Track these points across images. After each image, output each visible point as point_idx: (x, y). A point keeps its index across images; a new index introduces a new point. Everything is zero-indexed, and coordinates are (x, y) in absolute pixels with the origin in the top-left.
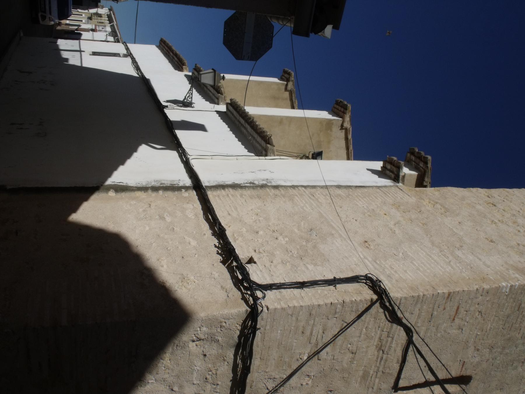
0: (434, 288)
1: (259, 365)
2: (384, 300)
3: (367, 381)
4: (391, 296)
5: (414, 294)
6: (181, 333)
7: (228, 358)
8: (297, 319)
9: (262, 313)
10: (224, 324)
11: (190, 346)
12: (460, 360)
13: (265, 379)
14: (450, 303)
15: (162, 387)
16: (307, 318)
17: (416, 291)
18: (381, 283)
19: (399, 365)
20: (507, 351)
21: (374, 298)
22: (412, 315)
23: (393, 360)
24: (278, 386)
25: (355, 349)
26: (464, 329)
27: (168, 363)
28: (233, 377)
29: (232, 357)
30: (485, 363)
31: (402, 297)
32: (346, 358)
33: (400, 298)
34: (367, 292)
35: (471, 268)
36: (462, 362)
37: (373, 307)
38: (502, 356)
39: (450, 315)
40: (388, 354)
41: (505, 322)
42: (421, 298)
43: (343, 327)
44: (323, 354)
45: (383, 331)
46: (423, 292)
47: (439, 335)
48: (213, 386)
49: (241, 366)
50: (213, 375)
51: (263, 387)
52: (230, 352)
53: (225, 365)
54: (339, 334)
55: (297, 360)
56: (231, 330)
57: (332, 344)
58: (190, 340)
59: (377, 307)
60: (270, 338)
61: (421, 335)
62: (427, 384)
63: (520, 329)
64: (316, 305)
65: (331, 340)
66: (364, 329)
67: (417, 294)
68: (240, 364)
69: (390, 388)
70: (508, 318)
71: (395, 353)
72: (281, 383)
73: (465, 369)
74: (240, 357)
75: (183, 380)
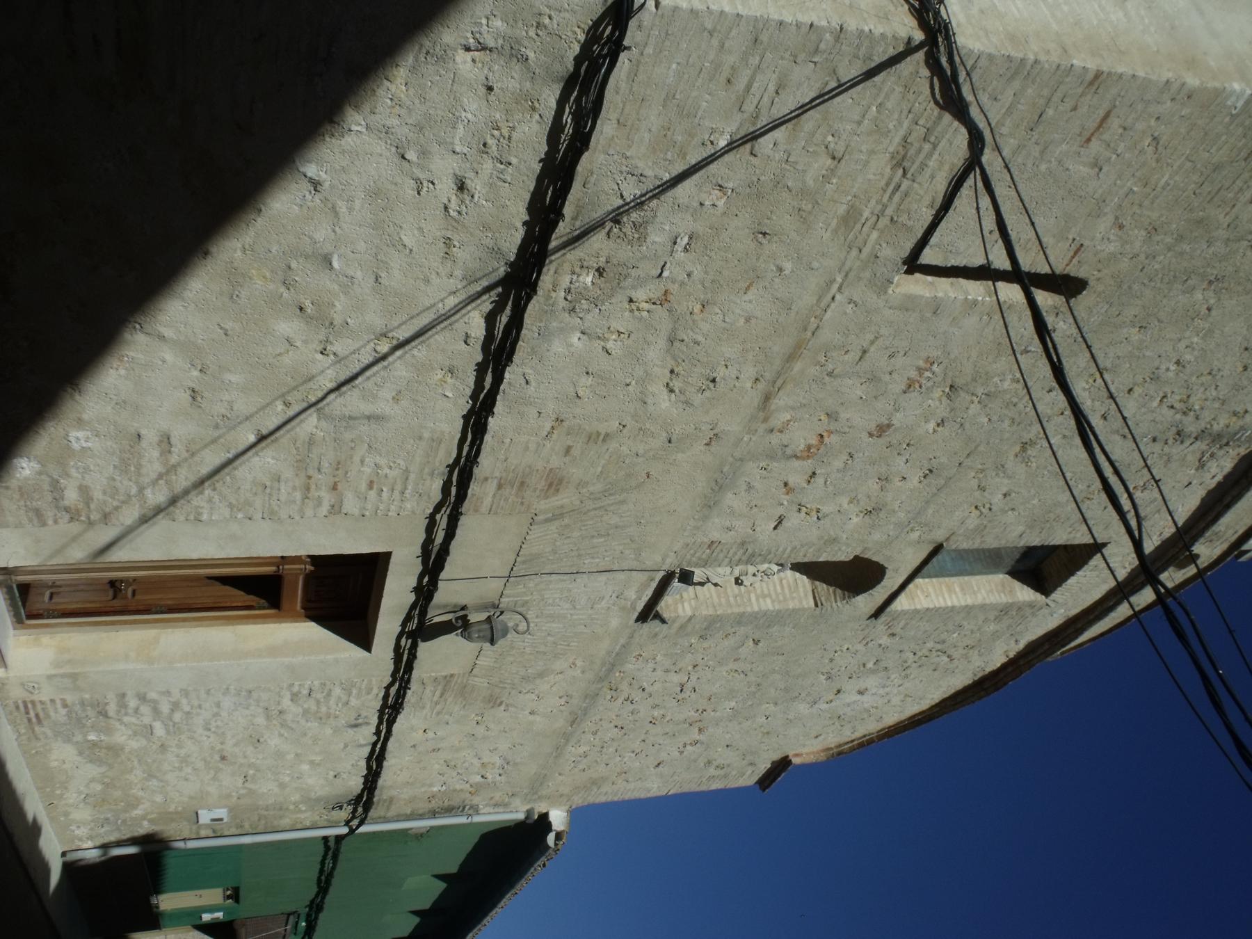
0: (1066, 51)
1: (613, 137)
2: (937, 47)
3: (852, 230)
4: (958, 44)
5: (1013, 54)
6: (442, 25)
7: (543, 105)
8: (722, 46)
9: (642, 11)
10: (547, 21)
11: (458, 59)
12: (1074, 240)
13: (621, 172)
14: (1093, 97)
15: (381, 147)
16: (746, 48)
17: (1021, 47)
18: (942, 5)
19: (934, 212)
20: (1186, 248)
21: (916, 38)
22: (994, 103)
23: (922, 197)
24: (647, 196)
25: (843, 149)
26: (1105, 169)
27: (402, 91)
28: (546, 154)
29: (553, 103)
30: (1126, 260)
31: (983, 52)
32: (816, 165)
33: (978, 53)
34: (903, 19)
35: (1172, 28)
36: (1077, 244)
37: (909, 58)
38: (1169, 255)
39: (1083, 128)
40: (914, 181)
41: (1206, 179)
42: (1028, 67)
43: (826, 90)
44: (765, 142)
45: (916, 124)
46: (1036, 54)
47: (1043, 167)
48: (499, 165)
49: (571, 131)
50: (501, 140)
51: (613, 190)
52: (550, 93)
53: (534, 120)
54: (813, 104)
55: (703, 144)
56: (561, 38)
57: (790, 125)
58: (461, 45)
59: (918, 63)
60: (649, 78)
61: (1004, 154)
62: (984, 273)
63: (1234, 206)
64: (773, 21)
65: (790, 116)
66: (874, 108)
67: (1021, 55)
68: (568, 126)
69: (899, 259)
70: (1214, 171)
71: (931, 183)
72: (655, 189)
73: (1079, 262)
74: (571, 109)
75: (432, 137)
